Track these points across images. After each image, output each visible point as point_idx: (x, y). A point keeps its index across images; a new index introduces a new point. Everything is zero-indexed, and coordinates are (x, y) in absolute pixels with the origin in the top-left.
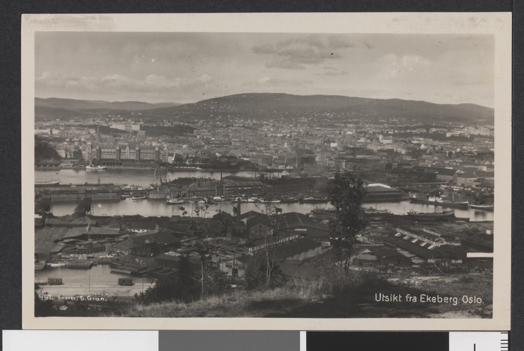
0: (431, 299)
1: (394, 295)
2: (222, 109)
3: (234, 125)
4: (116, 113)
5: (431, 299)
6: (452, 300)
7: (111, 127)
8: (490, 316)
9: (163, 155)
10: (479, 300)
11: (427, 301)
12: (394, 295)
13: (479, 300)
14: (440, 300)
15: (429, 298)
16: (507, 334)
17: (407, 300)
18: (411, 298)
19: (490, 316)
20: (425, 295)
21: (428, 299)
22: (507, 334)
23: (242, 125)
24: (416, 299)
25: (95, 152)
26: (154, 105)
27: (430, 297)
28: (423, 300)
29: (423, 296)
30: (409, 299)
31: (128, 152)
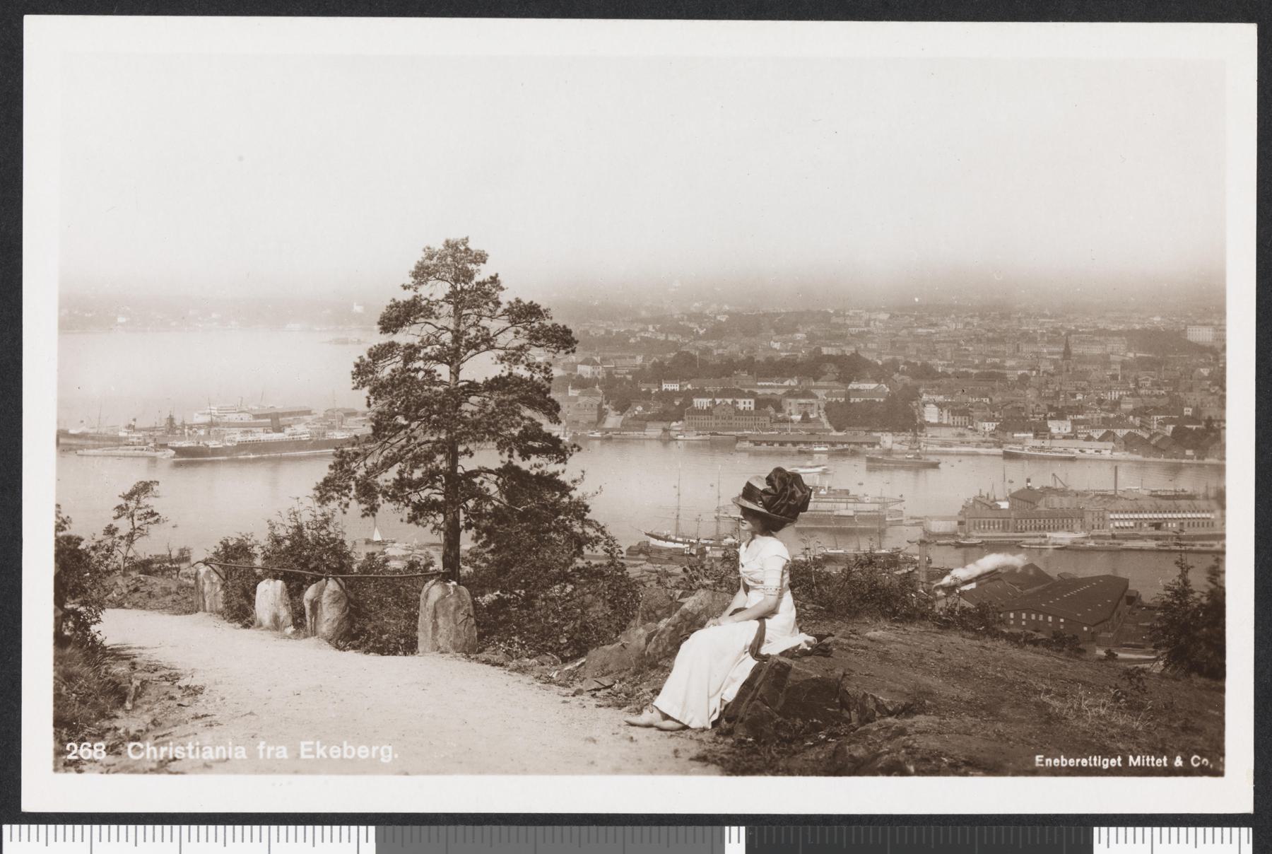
0: (327, 752)
6: (378, 752)
11: (318, 757)
14: (349, 752)
15: (321, 747)
16: (1246, 833)
18: (270, 749)
20: (311, 743)
22: (1246, 833)
23: (888, 315)
24: (303, 750)
27: (325, 747)
28: (307, 753)
29: (306, 746)
30: (265, 751)
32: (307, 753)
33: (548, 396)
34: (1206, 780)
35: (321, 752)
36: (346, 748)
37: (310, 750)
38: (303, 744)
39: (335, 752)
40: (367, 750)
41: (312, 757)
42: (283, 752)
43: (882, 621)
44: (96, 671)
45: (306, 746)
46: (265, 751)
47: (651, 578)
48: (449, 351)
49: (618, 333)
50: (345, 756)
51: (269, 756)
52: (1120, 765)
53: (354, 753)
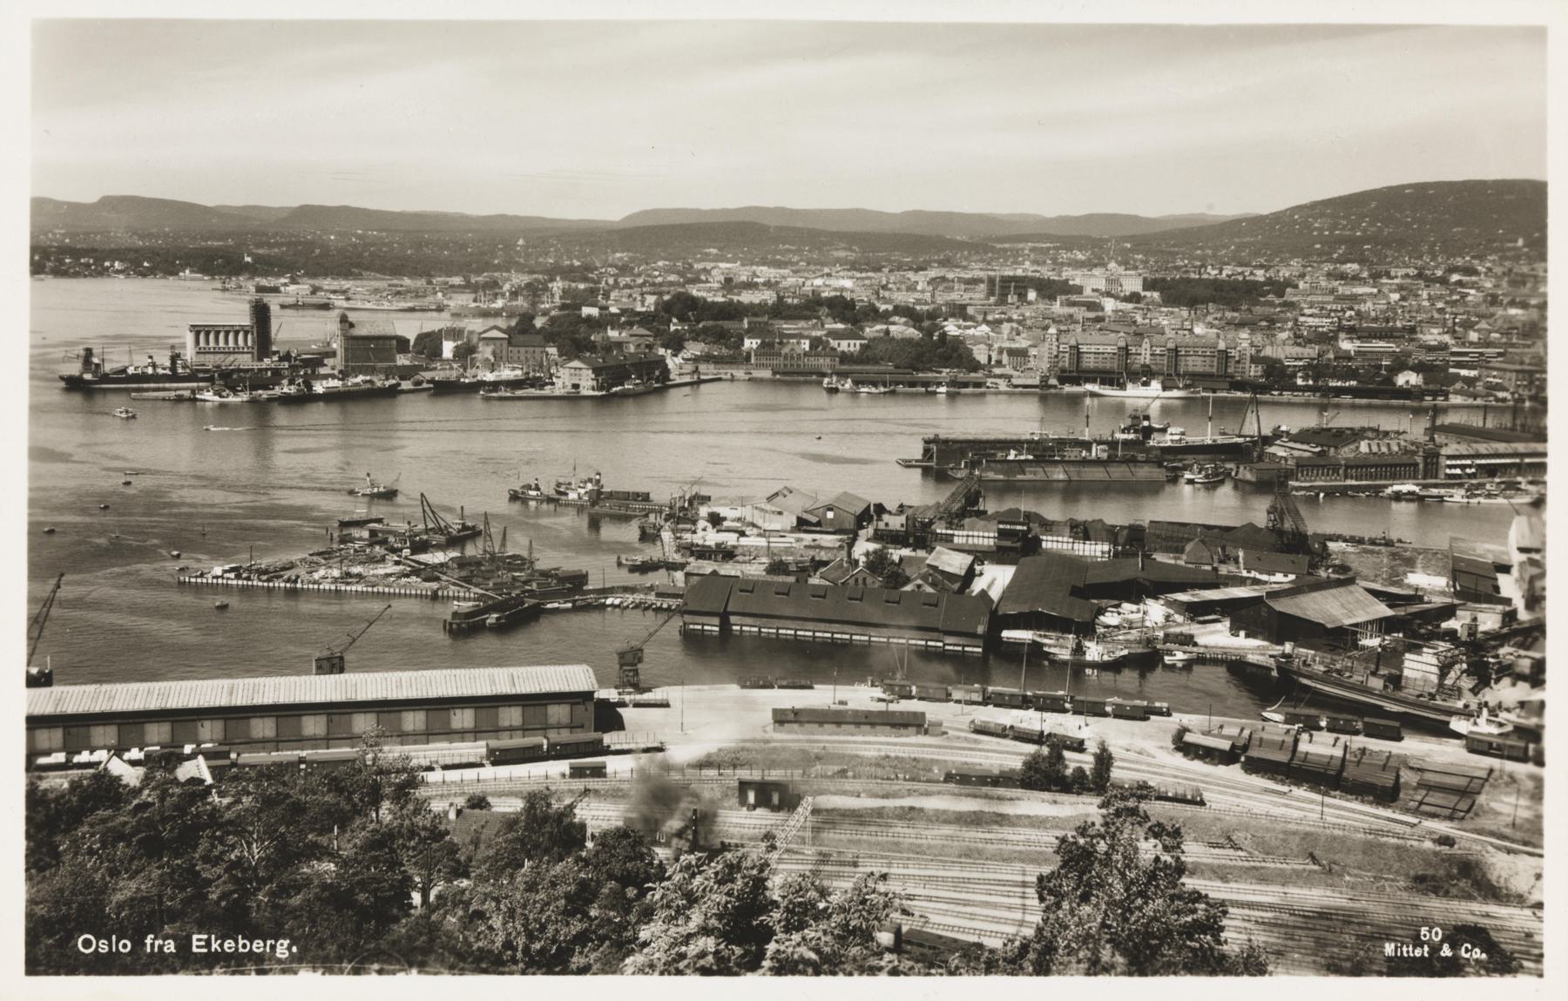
0: (221, 945)
1: (114, 937)
2: (1345, 226)
3: (1393, 274)
4: (1069, 243)
5: (221, 945)
7: (1071, 283)
8: (36, 965)
9: (1238, 362)
10: (125, 946)
12: (114, 937)
13: (125, 946)
14: (244, 946)
17: (149, 950)
19: (36, 965)
20: (205, 937)
21: (215, 946)
23: (1416, 272)
24: (195, 943)
25: (503, 545)
26: (1154, 220)
28: (198, 947)
29: (199, 940)
30: (152, 945)
31: (1148, 352)
32: (198, 947)
33: (1431, 413)
34: (1246, 980)
35: (215, 946)
36: (241, 942)
37: (203, 943)
38: (195, 937)
39: (229, 945)
40: (262, 944)
41: (205, 950)
42: (125, 946)
43: (620, 823)
44: (1138, 815)
45: (199, 940)
46: (152, 945)
47: (1225, 731)
48: (993, 295)
49: (1173, 279)
50: (241, 950)
51: (156, 950)
52: (1426, 955)
53: (255, 945)
